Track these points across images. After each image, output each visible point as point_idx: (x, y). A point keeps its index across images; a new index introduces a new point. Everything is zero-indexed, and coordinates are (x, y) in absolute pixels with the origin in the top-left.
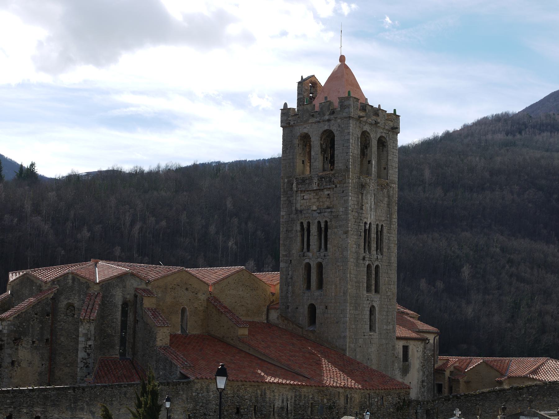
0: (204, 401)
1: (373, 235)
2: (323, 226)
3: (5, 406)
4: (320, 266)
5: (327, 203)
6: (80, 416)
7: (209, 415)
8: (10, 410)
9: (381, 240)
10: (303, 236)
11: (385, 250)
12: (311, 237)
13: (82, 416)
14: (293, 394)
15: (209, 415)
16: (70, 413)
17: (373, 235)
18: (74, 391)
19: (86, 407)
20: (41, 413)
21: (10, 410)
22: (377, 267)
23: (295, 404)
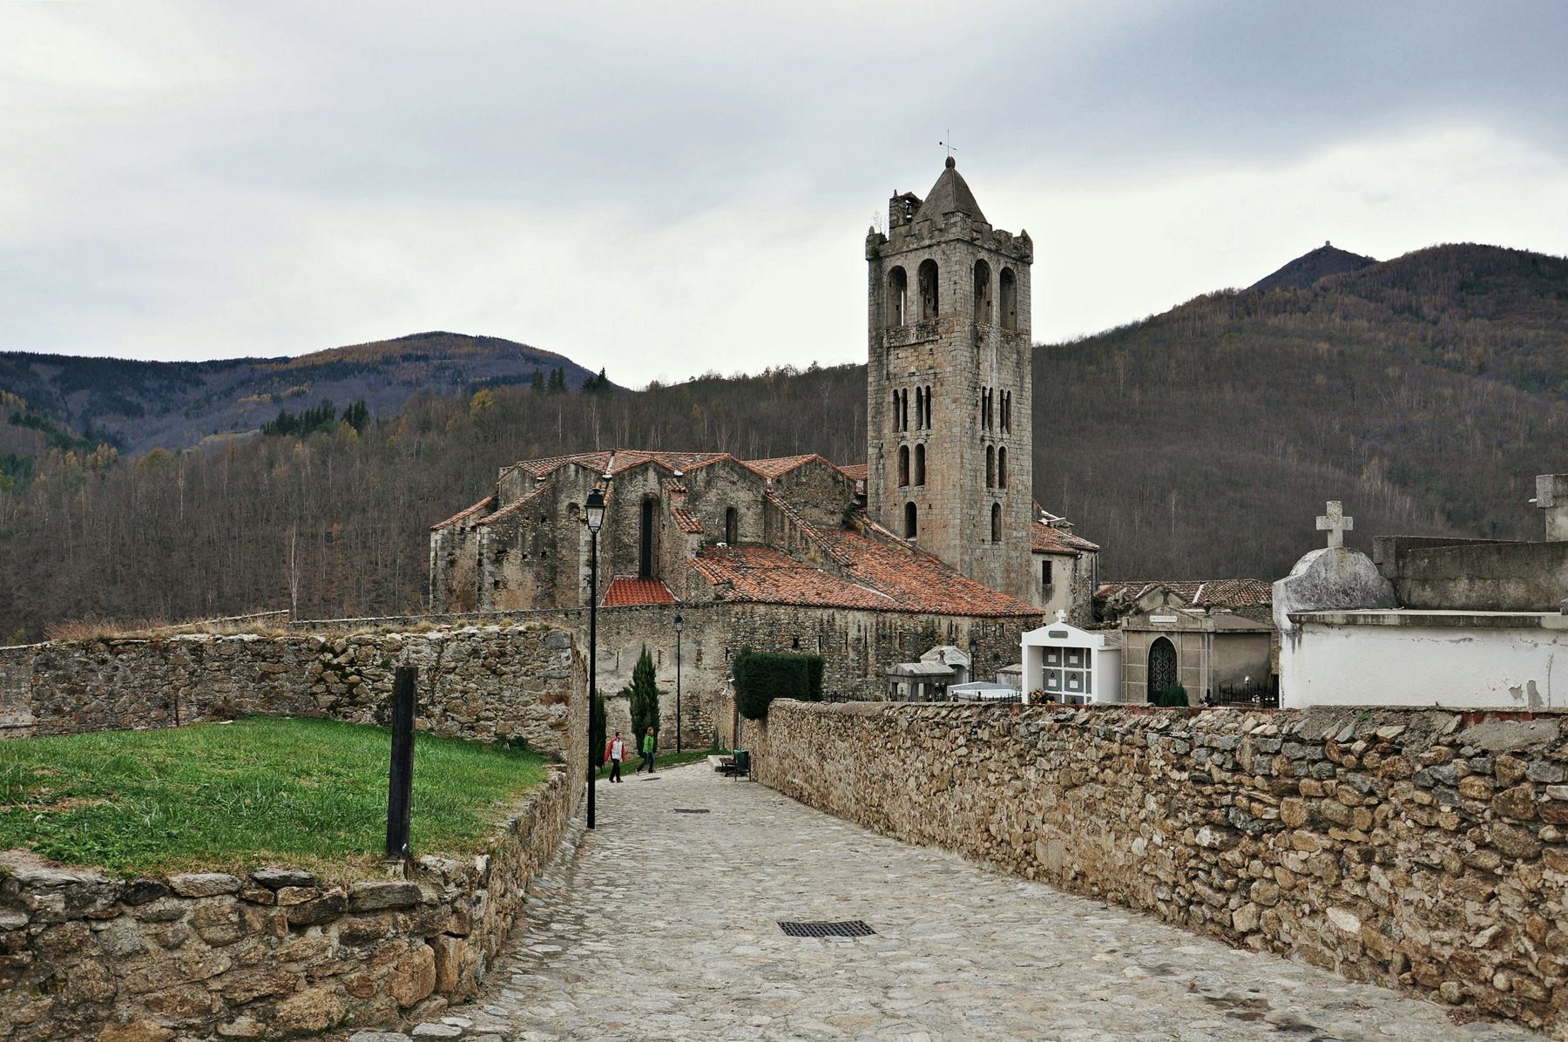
1: (996, 406)
5: (930, 362)
9: (1008, 414)
10: (897, 409)
11: (1014, 426)
17: (996, 406)
22: (1002, 450)
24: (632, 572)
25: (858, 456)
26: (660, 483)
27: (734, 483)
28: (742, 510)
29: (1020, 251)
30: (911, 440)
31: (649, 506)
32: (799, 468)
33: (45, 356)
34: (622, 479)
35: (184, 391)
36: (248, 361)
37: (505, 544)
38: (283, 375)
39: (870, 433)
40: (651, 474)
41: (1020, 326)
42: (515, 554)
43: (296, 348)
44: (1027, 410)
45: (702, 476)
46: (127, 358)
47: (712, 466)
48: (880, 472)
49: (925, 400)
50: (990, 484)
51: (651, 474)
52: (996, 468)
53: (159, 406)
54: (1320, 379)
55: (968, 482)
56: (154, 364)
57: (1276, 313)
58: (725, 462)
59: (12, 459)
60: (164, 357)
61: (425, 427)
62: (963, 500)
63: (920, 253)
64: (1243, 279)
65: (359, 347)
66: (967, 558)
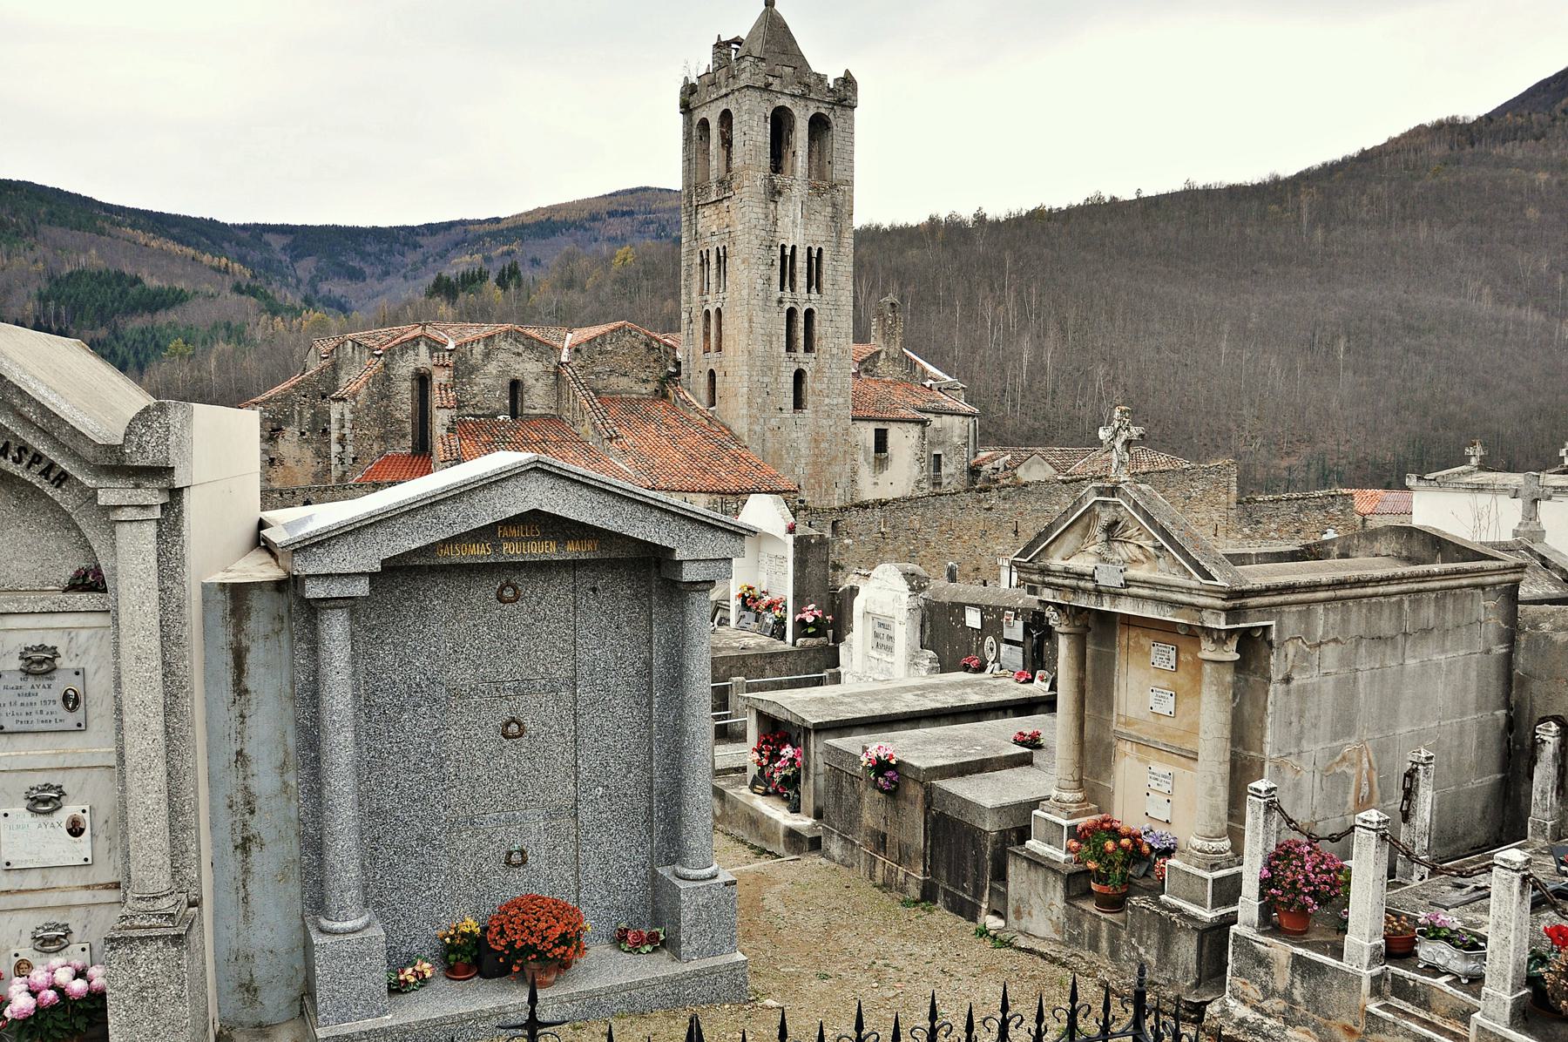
24: (405, 446)
25: (672, 325)
26: (432, 357)
27: (519, 354)
28: (529, 382)
29: (844, 93)
31: (422, 380)
32: (603, 335)
33: (276, 226)
34: (393, 355)
35: (403, 255)
36: (462, 223)
37: (280, 422)
38: (493, 235)
39: (684, 297)
40: (423, 349)
41: (837, 173)
42: (291, 432)
43: (509, 206)
44: (847, 266)
45: (479, 349)
46: (349, 224)
47: (491, 337)
48: (691, 342)
49: (722, 260)
50: (790, 346)
51: (423, 349)
52: (800, 330)
53: (379, 269)
54: (1532, 213)
55: (759, 348)
56: (375, 229)
57: (1504, 141)
58: (507, 333)
59: (228, 326)
60: (384, 223)
61: (570, 284)
62: (751, 367)
63: (719, 103)
64: (1474, 104)
65: (567, 205)
66: (757, 428)
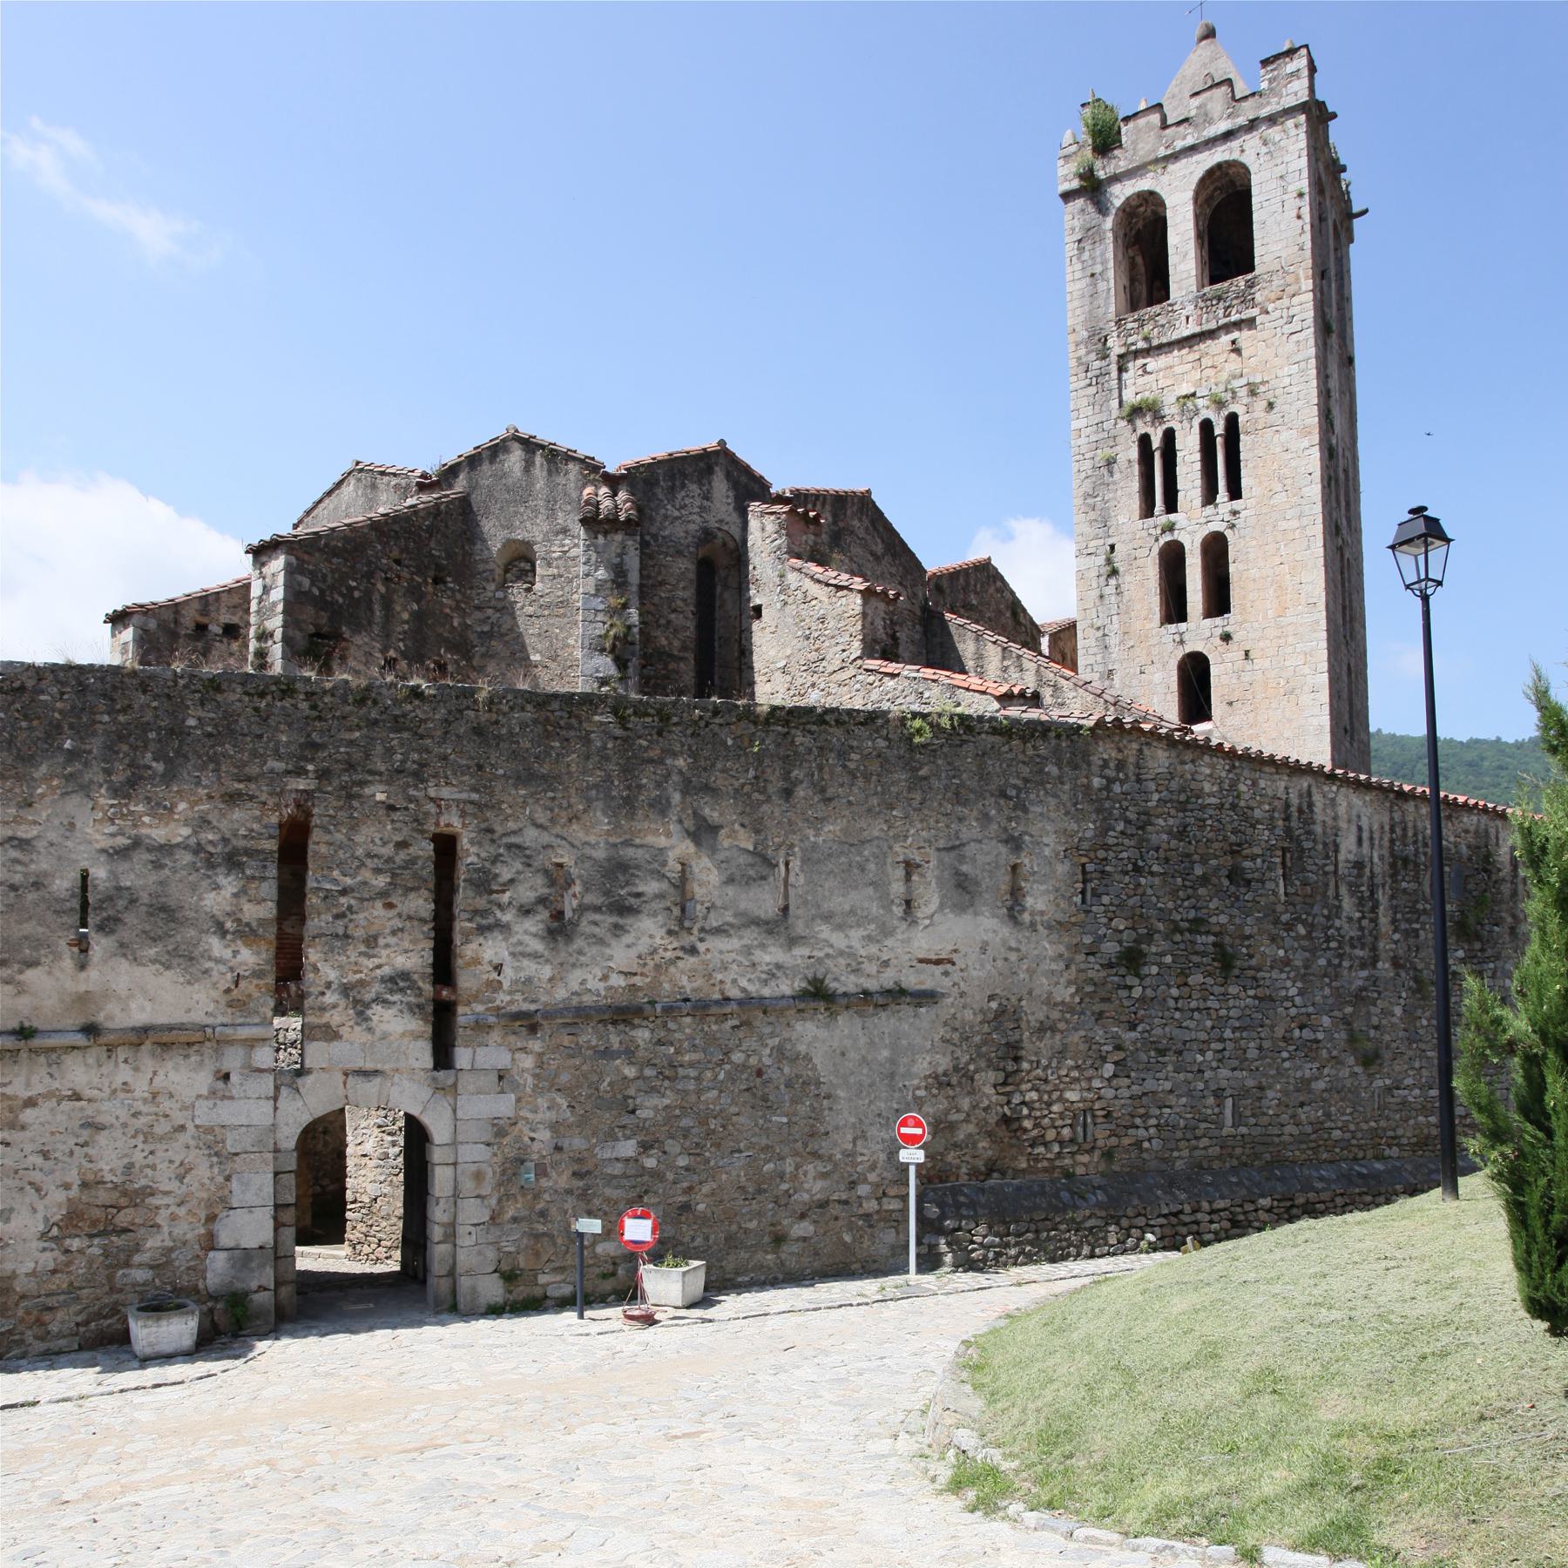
0: (1132, 815)
2: (1219, 429)
3: (273, 764)
4: (1216, 549)
6: (650, 839)
7: (1152, 874)
8: (302, 784)
12: (1180, 470)
13: (662, 841)
14: (1386, 820)
15: (1152, 874)
16: (604, 824)
18: (622, 721)
19: (676, 797)
20: (463, 814)
21: (302, 784)
23: (1392, 854)
27: (877, 558)
30: (1193, 523)
